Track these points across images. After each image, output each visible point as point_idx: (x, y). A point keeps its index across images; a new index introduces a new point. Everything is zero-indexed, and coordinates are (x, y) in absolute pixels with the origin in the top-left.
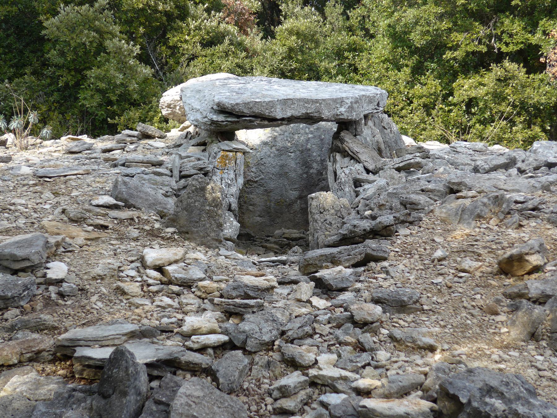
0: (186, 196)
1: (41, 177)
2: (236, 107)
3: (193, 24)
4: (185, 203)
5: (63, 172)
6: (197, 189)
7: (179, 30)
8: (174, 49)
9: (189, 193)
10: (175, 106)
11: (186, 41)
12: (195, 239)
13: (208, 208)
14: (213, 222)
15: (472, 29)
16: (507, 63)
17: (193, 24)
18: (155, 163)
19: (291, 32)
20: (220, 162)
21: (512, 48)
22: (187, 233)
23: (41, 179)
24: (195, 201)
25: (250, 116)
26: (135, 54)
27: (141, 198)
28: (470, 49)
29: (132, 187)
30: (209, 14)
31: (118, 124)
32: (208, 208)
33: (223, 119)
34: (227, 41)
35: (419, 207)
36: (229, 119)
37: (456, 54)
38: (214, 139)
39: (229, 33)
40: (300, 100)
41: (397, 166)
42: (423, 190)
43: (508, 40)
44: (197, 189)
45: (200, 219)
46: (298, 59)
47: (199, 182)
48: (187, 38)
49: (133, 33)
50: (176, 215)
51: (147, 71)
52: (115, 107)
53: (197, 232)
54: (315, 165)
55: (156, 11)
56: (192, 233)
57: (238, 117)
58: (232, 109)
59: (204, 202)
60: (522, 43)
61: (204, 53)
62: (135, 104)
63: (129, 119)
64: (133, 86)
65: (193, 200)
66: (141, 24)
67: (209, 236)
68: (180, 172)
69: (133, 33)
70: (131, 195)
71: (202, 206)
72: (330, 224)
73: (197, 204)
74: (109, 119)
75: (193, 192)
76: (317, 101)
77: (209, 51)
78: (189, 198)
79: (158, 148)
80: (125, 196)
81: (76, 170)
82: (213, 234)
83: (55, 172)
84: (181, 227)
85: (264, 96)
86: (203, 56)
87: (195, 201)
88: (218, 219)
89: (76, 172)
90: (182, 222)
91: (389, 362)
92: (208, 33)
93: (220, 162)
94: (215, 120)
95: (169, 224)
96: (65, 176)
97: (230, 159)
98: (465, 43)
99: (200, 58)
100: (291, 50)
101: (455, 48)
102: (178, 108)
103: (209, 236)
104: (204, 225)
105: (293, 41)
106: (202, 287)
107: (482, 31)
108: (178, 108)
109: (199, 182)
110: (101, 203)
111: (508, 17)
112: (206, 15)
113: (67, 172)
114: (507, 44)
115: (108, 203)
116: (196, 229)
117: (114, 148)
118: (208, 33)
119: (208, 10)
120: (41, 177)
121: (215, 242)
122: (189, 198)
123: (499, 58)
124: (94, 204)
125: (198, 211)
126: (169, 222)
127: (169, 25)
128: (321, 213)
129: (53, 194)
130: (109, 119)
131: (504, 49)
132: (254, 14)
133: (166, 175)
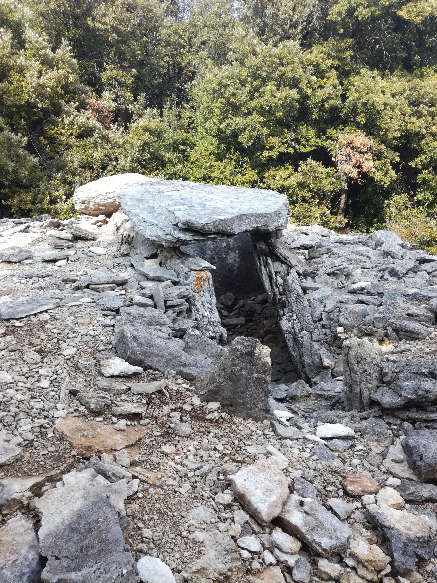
0: (230, 364)
1: (8, 320)
2: (206, 227)
3: (67, 120)
4: (229, 372)
5: (31, 310)
6: (242, 354)
7: (55, 124)
8: (52, 140)
9: (234, 360)
10: (89, 202)
11: (62, 134)
12: (241, 412)
13: (256, 376)
14: (261, 391)
15: (283, 134)
16: (310, 161)
17: (67, 120)
18: (119, 283)
19: (146, 129)
20: (196, 285)
21: (308, 149)
22: (231, 405)
23: (9, 324)
24: (241, 369)
25: (215, 234)
26: (23, 145)
27: (156, 355)
28: (282, 150)
29: (143, 341)
30: (79, 111)
31: (11, 206)
32: (256, 376)
33: (191, 238)
34: (96, 135)
35: (420, 336)
36: (197, 238)
37: (272, 153)
38: (173, 254)
39: (96, 128)
40: (252, 215)
41: (328, 271)
42: (409, 315)
43: (305, 143)
44: (242, 354)
45: (247, 389)
46: (149, 151)
47: (245, 346)
48: (63, 131)
49: (14, 124)
50: (218, 387)
51: (35, 160)
52: (7, 190)
53: (243, 403)
54: (209, 252)
55: (36, 107)
56: (238, 405)
57: (203, 235)
58: (201, 229)
59: (251, 370)
60: (315, 145)
61: (78, 144)
62: (27, 188)
63: (21, 201)
64: (24, 173)
65: (238, 368)
66: (22, 117)
67: (256, 407)
68: (166, 301)
69: (14, 124)
70: (146, 354)
71: (249, 373)
72: (370, 375)
73: (243, 373)
74: (3, 201)
75: (238, 358)
76: (265, 216)
77: (82, 143)
78: (233, 365)
79: (100, 255)
80: (140, 356)
81: (46, 304)
82: (260, 405)
83: (22, 311)
84: (224, 399)
85: (215, 210)
86: (77, 146)
87: (241, 369)
88: (267, 387)
89: (45, 308)
90: (226, 393)
91: (324, 442)
92: (80, 127)
93: (196, 285)
94: (183, 239)
95: (209, 397)
96: (35, 315)
97: (204, 281)
98: (277, 145)
99: (74, 148)
100: (146, 143)
101: (271, 149)
102: (92, 204)
103: (256, 407)
104: (252, 395)
105: (147, 137)
106: (367, 561)
107: (290, 136)
108: (92, 204)
109: (245, 346)
110: (116, 373)
111: (303, 125)
112: (76, 112)
113: (36, 309)
114: (304, 146)
115: (125, 373)
116: (242, 401)
117: (58, 258)
118: (80, 127)
119: (78, 109)
120: (8, 320)
121: (262, 413)
122: (233, 365)
123: (304, 157)
124: (108, 375)
125: (245, 381)
126: (209, 395)
127: (46, 119)
128: (359, 362)
129: (38, 352)
130: (3, 201)
131: (303, 150)
132: (112, 112)
133: (150, 305)
